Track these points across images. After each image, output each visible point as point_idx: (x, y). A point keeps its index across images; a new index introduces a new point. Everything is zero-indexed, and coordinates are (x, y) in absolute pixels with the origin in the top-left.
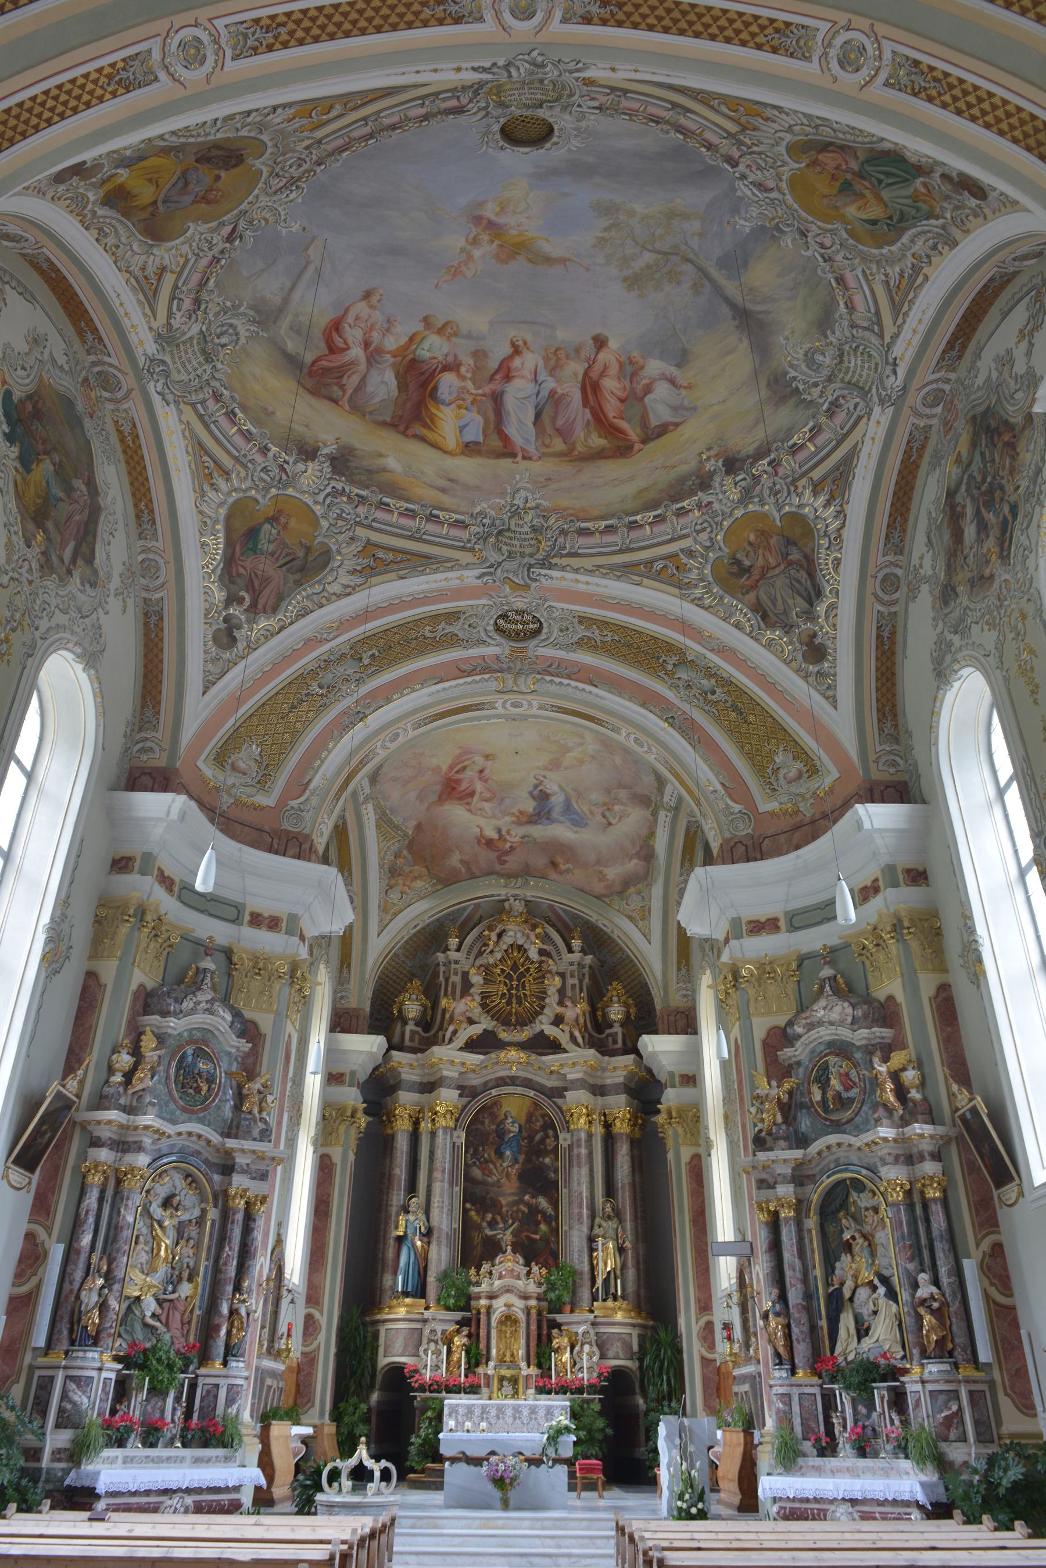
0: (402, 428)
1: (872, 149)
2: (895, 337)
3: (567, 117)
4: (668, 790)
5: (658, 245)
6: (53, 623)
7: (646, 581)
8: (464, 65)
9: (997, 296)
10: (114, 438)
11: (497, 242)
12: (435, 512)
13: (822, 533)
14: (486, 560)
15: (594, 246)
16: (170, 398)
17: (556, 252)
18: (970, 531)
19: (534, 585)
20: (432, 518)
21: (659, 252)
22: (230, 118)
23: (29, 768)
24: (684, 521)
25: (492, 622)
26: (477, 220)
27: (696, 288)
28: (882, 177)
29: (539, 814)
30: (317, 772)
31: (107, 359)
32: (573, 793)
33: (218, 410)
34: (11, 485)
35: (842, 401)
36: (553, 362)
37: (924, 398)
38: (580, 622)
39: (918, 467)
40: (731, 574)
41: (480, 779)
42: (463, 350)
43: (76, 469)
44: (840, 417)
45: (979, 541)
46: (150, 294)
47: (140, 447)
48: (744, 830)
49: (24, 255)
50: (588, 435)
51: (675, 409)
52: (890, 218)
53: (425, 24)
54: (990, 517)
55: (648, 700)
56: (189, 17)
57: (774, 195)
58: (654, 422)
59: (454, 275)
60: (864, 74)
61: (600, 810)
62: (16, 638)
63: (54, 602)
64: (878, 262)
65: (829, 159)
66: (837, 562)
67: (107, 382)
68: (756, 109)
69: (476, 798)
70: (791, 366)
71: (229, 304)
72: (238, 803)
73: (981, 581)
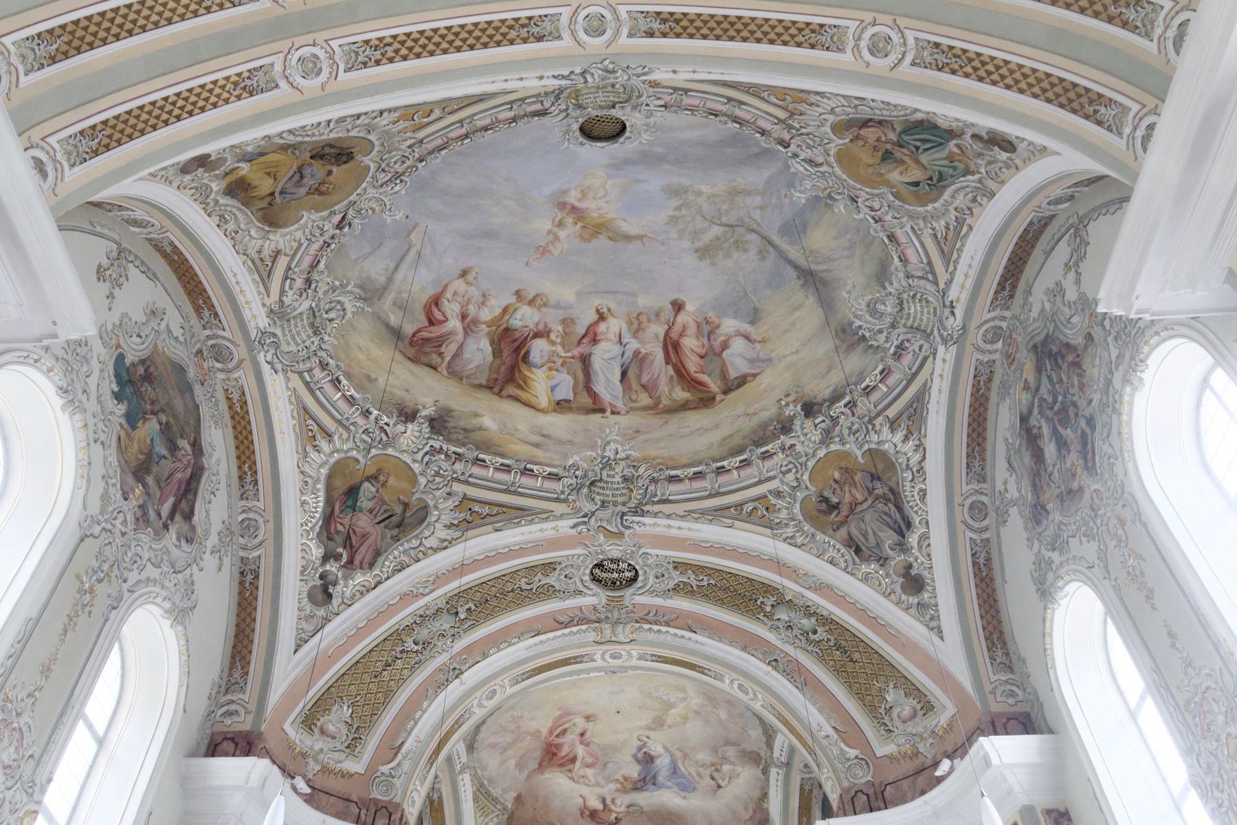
0: (496, 389)
1: (907, 121)
2: (949, 282)
3: (637, 115)
4: (779, 742)
5: (724, 220)
6: (143, 576)
7: (737, 523)
8: (546, 74)
9: (1037, 239)
10: (223, 406)
11: (580, 224)
12: (529, 466)
13: (904, 466)
14: (580, 510)
15: (667, 224)
16: (279, 366)
17: (634, 231)
18: (1050, 450)
19: (628, 532)
20: (526, 472)
21: (726, 225)
22: (342, 120)
23: (101, 732)
24: (769, 463)
25: (588, 572)
26: (562, 205)
27: (762, 254)
28: (918, 144)
29: (644, 779)
30: (409, 734)
31: (221, 333)
32: (678, 754)
33: (324, 378)
34: (114, 439)
35: (907, 344)
36: (635, 326)
37: (984, 335)
38: (675, 568)
39: (987, 399)
40: (820, 511)
41: (581, 743)
42: (553, 320)
43: (182, 431)
44: (907, 359)
45: (1062, 457)
46: (265, 275)
47: (247, 412)
48: (863, 777)
49: (150, 240)
50: (671, 390)
51: (752, 361)
52: (931, 179)
53: (512, 42)
54: (1068, 433)
55: (749, 643)
56: (309, 39)
57: (824, 168)
58: (733, 374)
59: (543, 254)
60: (893, 58)
61: (708, 772)
62: (101, 589)
63: (146, 555)
64: (924, 218)
65: (871, 134)
66: (923, 493)
67: (220, 354)
68: (802, 96)
69: (578, 764)
70: (856, 316)
71: (337, 283)
72: (326, 770)
73: (1070, 495)
